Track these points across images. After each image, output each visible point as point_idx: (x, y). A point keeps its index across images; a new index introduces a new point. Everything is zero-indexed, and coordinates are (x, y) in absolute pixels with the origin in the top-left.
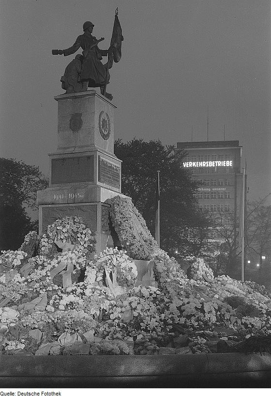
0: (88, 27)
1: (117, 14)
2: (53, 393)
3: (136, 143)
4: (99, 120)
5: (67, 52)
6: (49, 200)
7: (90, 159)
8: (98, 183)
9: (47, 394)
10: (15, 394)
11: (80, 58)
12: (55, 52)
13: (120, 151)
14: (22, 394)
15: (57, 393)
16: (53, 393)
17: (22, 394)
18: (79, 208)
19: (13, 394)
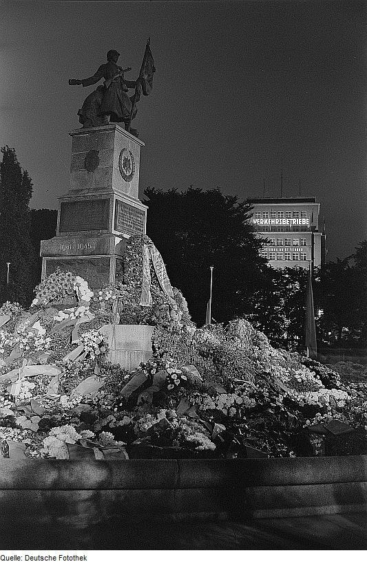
0: (112, 55)
1: (148, 44)
2: (75, 558)
3: (193, 194)
4: (120, 159)
5: (86, 83)
6: (55, 251)
7: (105, 203)
8: (114, 232)
9: (67, 558)
10: (21, 559)
11: (102, 90)
12: (73, 82)
13: (149, 196)
14: (31, 558)
15: (81, 557)
16: (75, 558)
17: (31, 558)
18: (90, 262)
19: (18, 558)
